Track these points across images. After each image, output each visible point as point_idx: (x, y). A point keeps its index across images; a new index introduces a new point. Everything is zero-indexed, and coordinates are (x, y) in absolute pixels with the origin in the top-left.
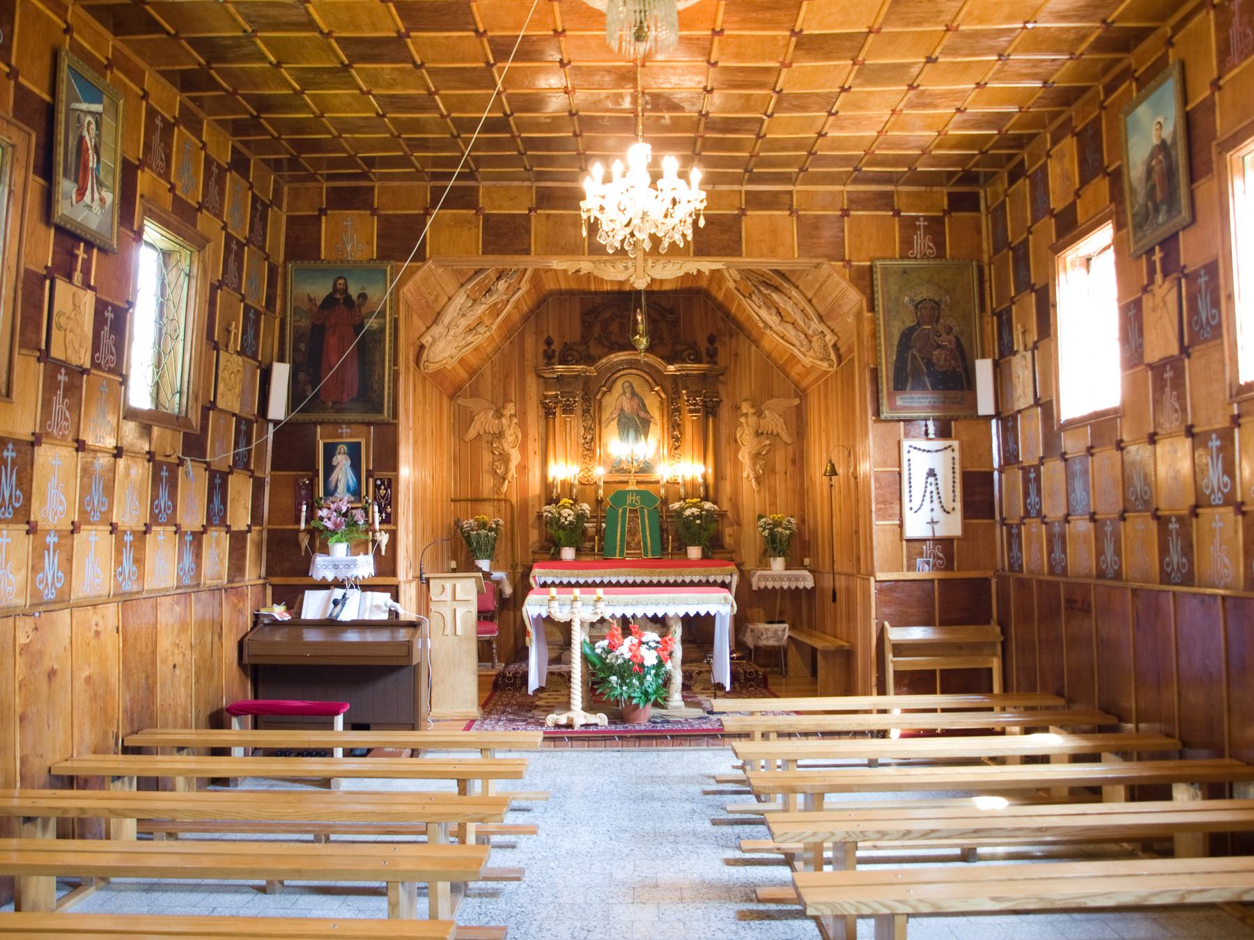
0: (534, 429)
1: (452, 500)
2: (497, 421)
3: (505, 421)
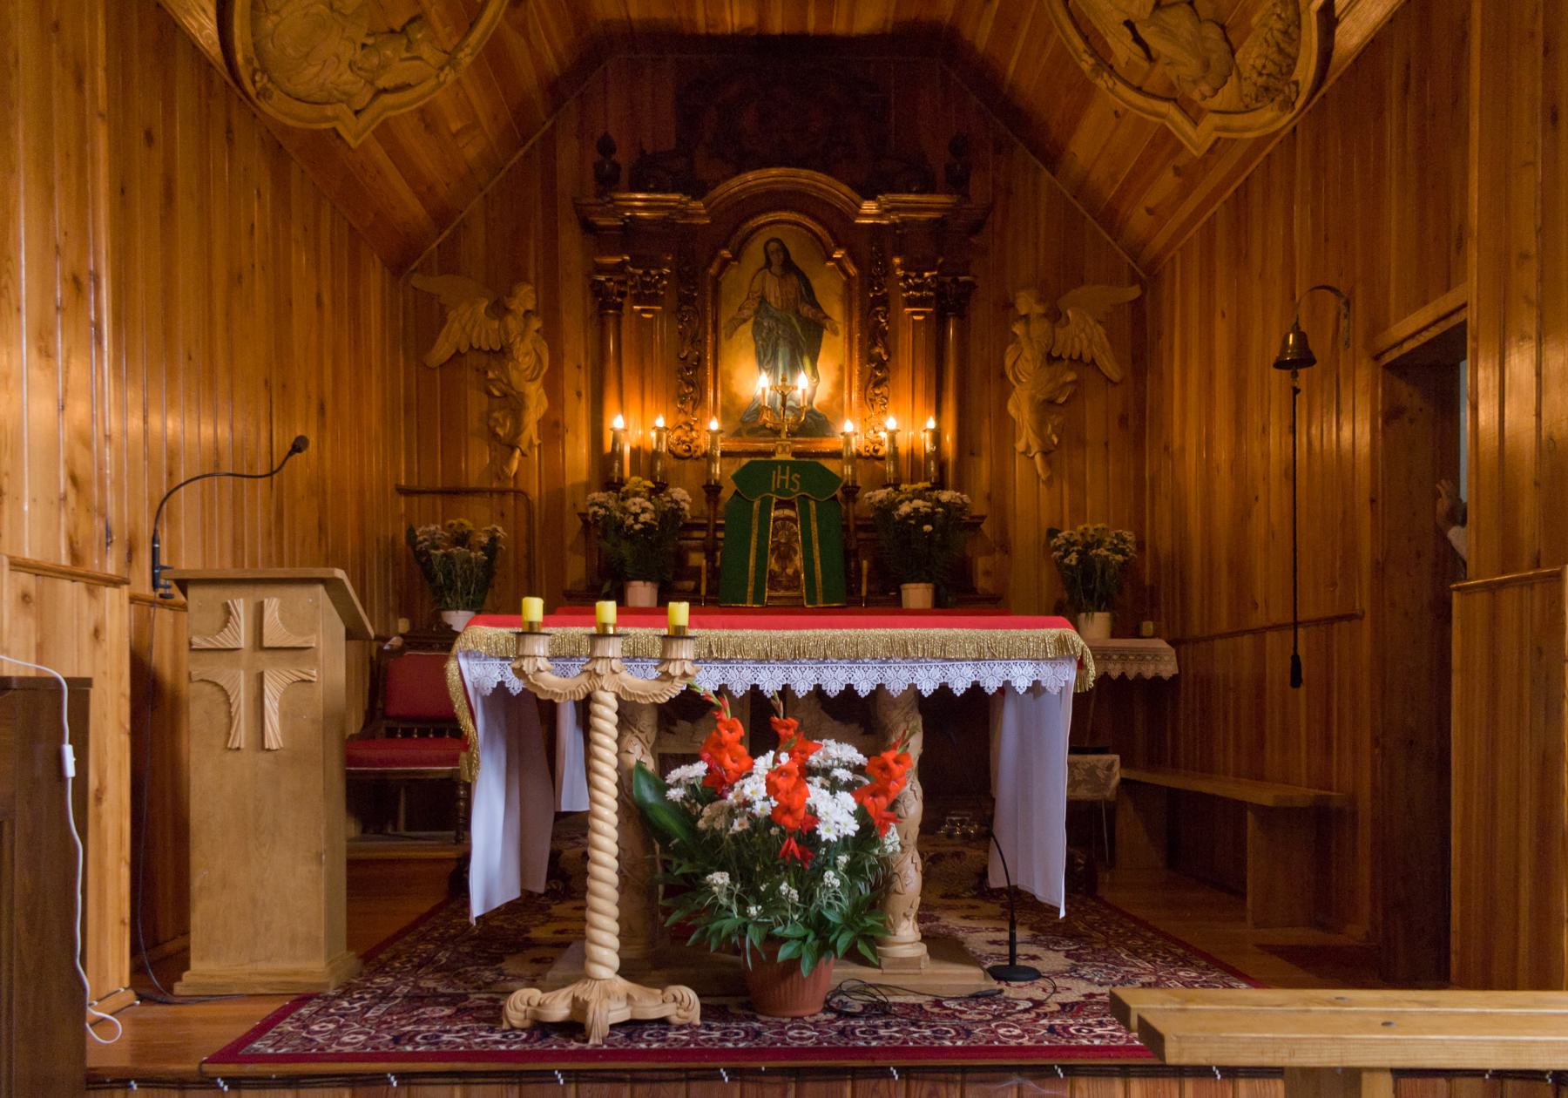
0: (576, 344)
2: (496, 324)
3: (513, 324)
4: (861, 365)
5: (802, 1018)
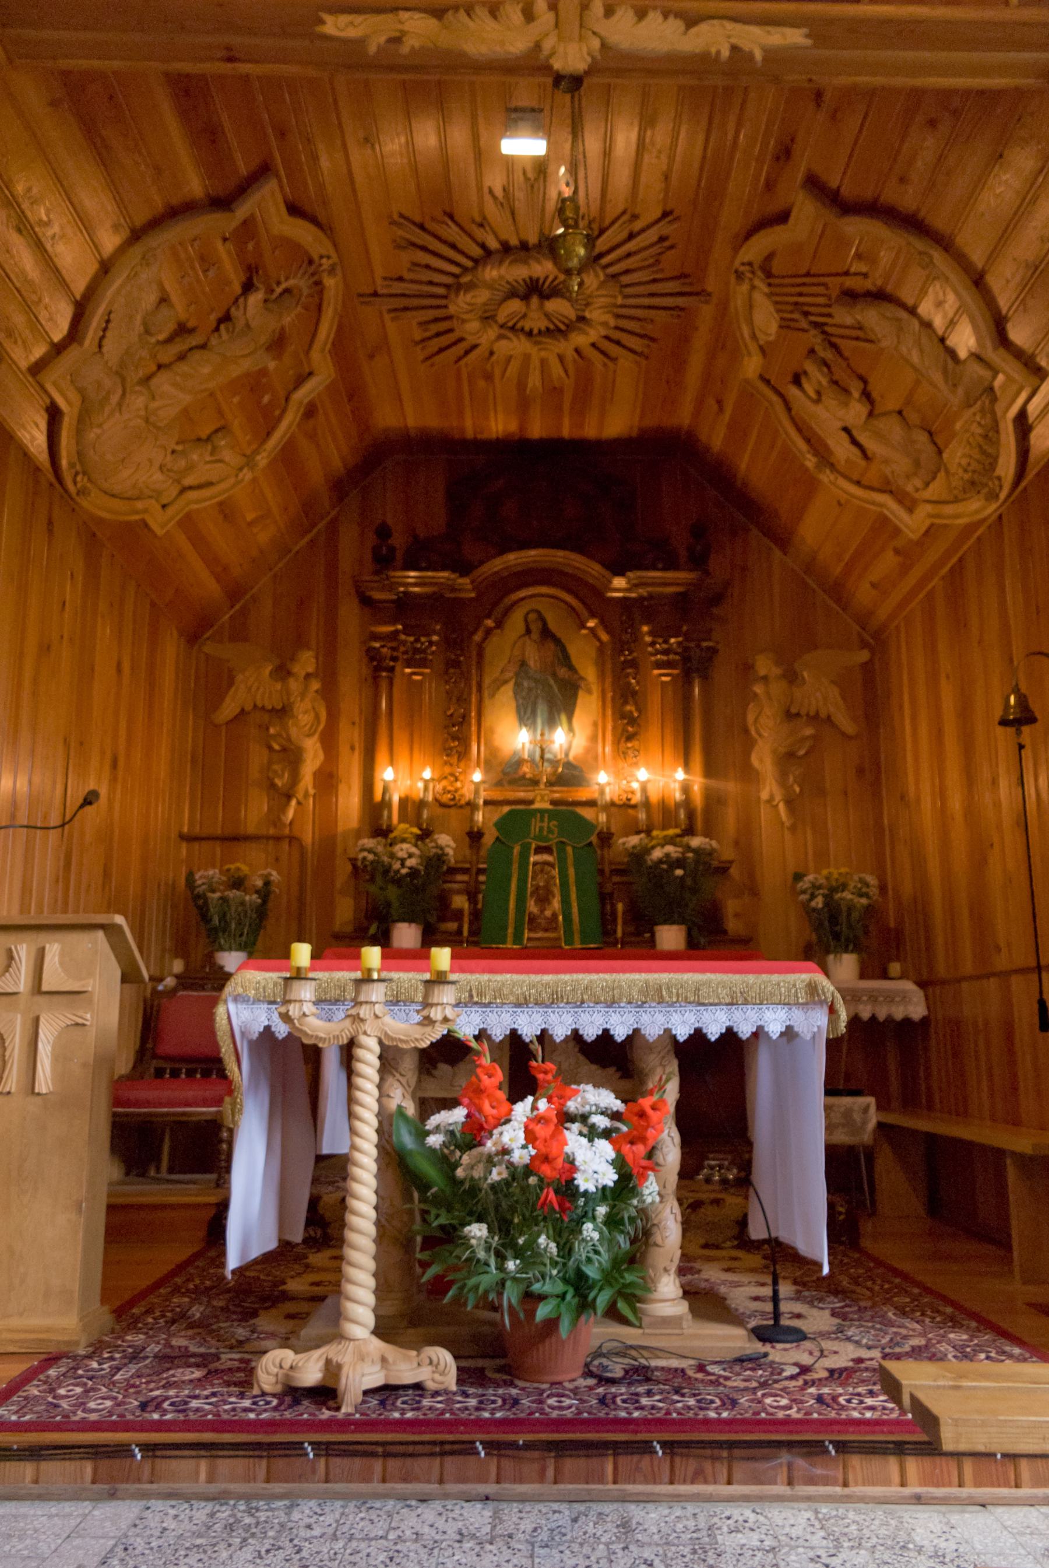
1: (182, 837)
2: (279, 686)
3: (294, 685)
4: (614, 721)
5: (560, 1383)
